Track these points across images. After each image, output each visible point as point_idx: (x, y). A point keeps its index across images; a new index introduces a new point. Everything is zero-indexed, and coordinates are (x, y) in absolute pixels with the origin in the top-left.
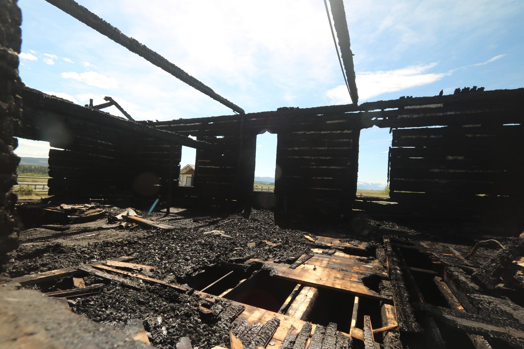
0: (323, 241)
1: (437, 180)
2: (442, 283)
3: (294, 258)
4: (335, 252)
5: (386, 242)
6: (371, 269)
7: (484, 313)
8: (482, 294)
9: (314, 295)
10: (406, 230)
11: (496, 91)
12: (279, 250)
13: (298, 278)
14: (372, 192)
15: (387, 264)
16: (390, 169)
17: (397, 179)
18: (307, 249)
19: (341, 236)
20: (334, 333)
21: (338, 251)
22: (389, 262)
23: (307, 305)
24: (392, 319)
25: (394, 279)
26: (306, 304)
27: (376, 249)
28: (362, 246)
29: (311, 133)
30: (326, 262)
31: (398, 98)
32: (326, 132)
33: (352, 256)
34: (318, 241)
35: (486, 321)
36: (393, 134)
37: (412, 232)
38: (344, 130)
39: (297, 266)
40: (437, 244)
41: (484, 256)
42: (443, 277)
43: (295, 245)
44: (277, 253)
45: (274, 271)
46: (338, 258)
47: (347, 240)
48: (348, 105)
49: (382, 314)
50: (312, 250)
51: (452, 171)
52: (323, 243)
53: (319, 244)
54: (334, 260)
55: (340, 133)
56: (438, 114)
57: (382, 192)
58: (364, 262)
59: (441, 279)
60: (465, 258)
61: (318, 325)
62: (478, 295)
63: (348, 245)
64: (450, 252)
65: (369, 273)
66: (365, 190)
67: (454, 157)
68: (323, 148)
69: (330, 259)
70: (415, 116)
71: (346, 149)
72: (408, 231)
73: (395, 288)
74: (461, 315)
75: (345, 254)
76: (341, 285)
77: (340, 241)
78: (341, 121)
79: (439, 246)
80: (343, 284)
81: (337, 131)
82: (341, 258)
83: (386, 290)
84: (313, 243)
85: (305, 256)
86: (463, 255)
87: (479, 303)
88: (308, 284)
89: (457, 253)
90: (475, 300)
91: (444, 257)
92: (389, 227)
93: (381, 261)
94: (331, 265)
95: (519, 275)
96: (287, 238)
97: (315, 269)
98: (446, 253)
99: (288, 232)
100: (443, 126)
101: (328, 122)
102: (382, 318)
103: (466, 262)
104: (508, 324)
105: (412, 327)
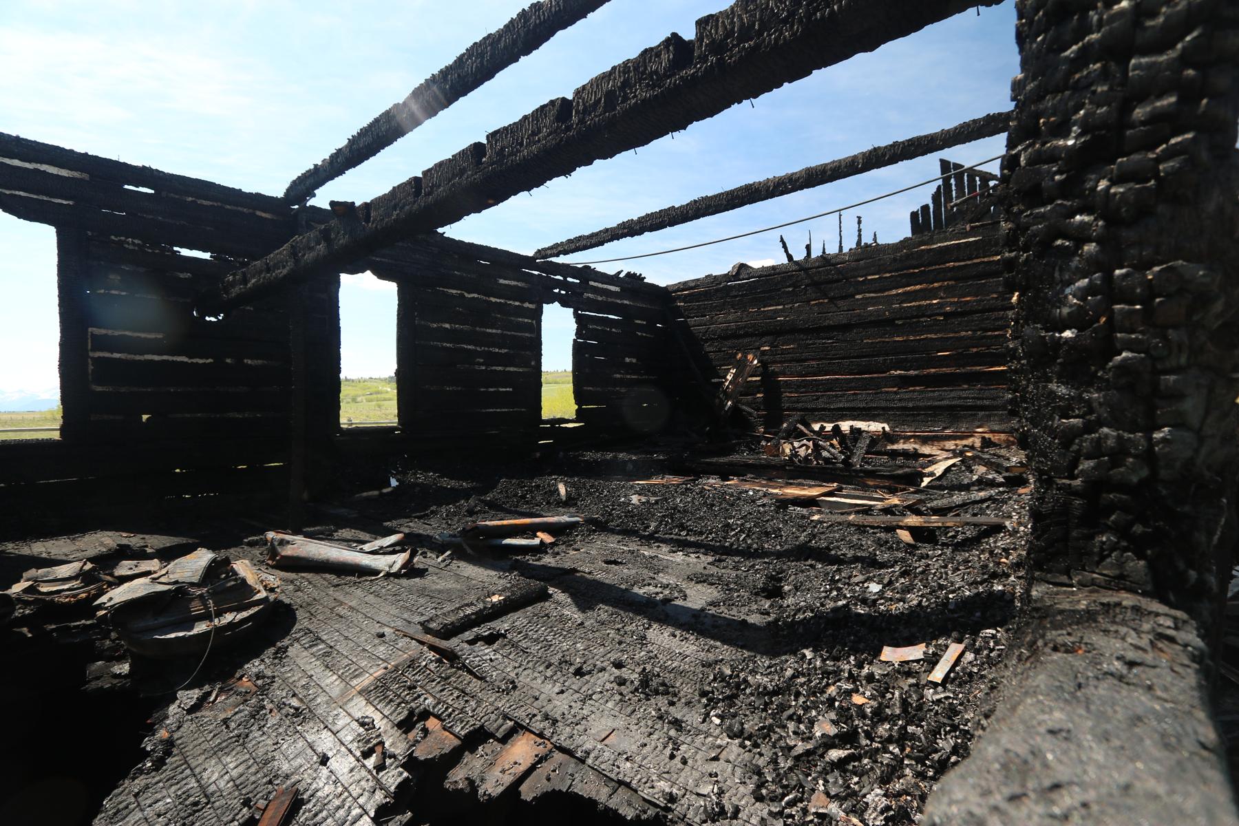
11: (197, 180)
57: (49, 416)
68: (494, 331)
81: (515, 300)
100: (616, 318)
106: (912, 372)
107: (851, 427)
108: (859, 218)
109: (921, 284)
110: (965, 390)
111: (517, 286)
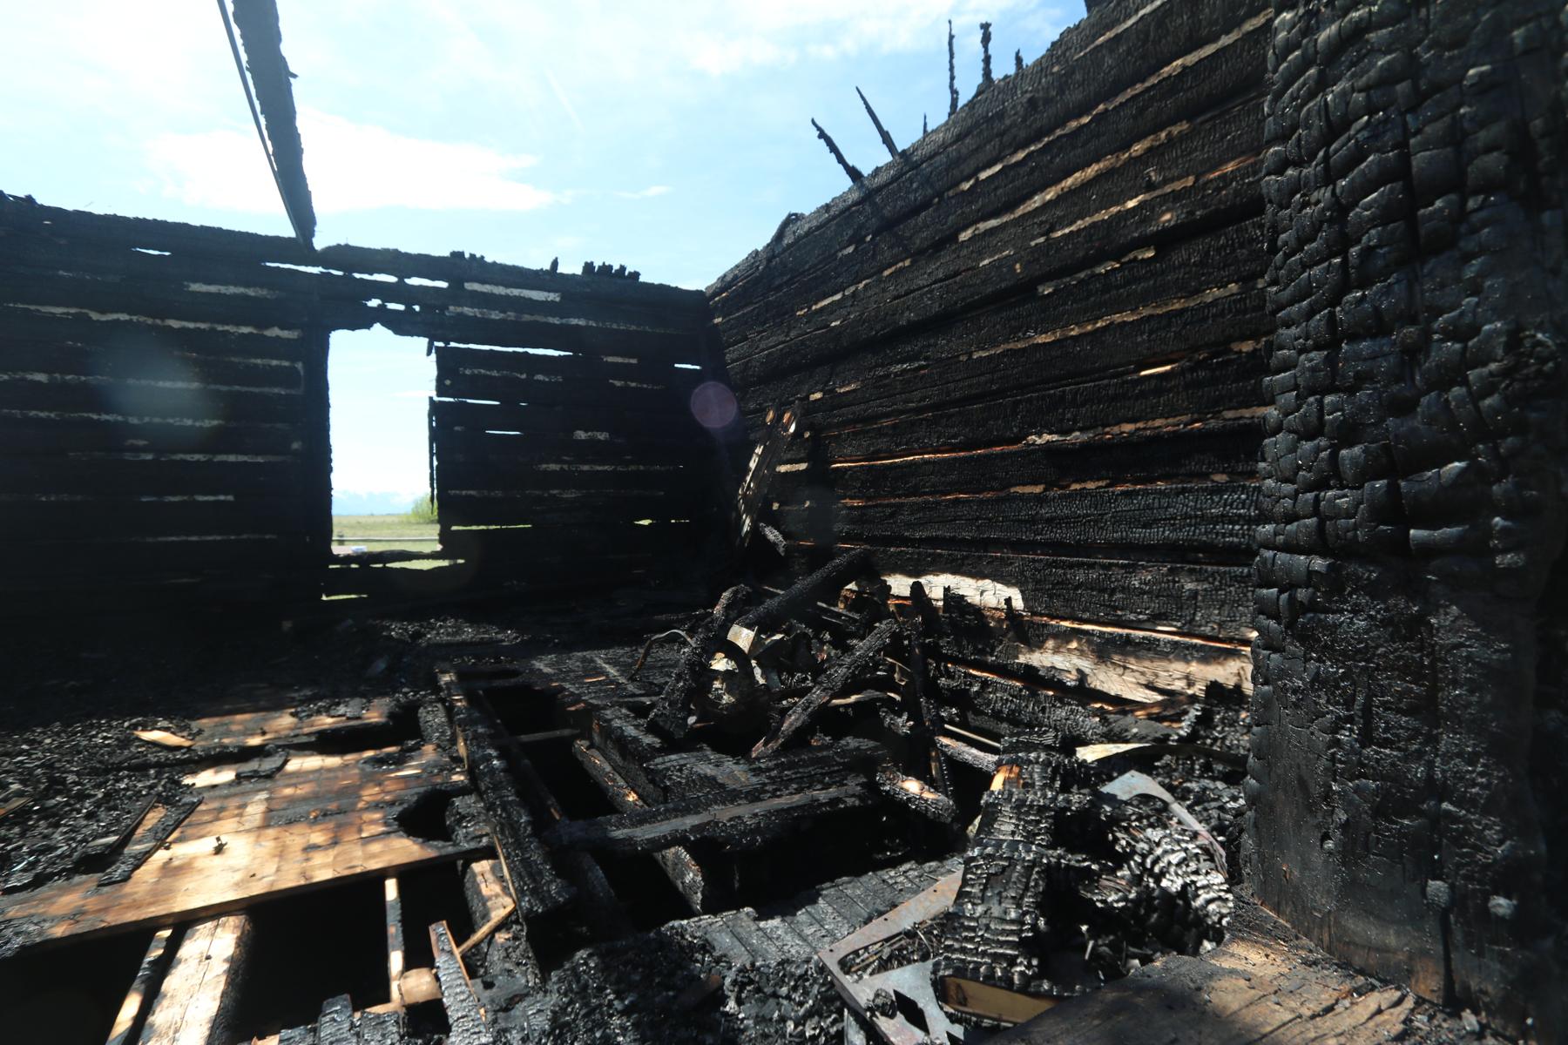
0: (228, 734)
1: (555, 492)
3: (112, 839)
4: (286, 762)
5: (446, 683)
6: (417, 777)
8: (667, 755)
9: (240, 942)
10: (493, 633)
12: (17, 830)
13: (153, 909)
14: (372, 520)
15: (461, 749)
16: (435, 463)
17: (458, 492)
18: (164, 786)
19: (293, 699)
20: (346, 1025)
21: (296, 756)
22: (465, 744)
23: (221, 987)
24: (497, 896)
25: (489, 788)
26: (215, 988)
27: (419, 707)
28: (375, 714)
29: (118, 320)
30: (262, 808)
31: (446, 254)
32: (191, 325)
33: (350, 757)
34: (206, 739)
35: (680, 811)
36: (437, 358)
37: (509, 636)
38: (267, 327)
39: (137, 867)
40: (570, 659)
41: (659, 664)
42: (590, 738)
43: (98, 786)
44: (9, 848)
45: (18, 930)
46: (301, 780)
47: (321, 707)
48: (277, 238)
49: (469, 893)
50: (188, 780)
51: (586, 468)
52: (226, 741)
53: (215, 748)
54: (288, 791)
55: (251, 334)
56: (551, 320)
57: (405, 520)
58: (391, 765)
59: (586, 743)
60: (628, 680)
61: (285, 1033)
63: (326, 722)
64: (599, 672)
65: (411, 795)
66: (347, 516)
67: (589, 433)
69: (271, 791)
70: (495, 315)
71: (283, 393)
72: (500, 636)
73: (495, 811)
74: (641, 819)
75: (324, 757)
76: (333, 865)
77: (293, 715)
78: (251, 292)
79: (574, 661)
80: (339, 859)
81: (238, 324)
82: (311, 777)
83: (469, 822)
84: (184, 754)
85: (166, 815)
86: (624, 671)
88: (203, 914)
89: (612, 671)
92: (448, 634)
93: (442, 744)
94: (281, 813)
95: (717, 689)
96: (48, 766)
97: (219, 850)
99: (48, 741)
100: (562, 353)
101: (196, 287)
102: (470, 905)
103: (631, 687)
105: (550, 895)
106: (1076, 437)
107: (947, 590)
108: (985, 27)
109: (1098, 161)
110: (1218, 490)
111: (246, 297)
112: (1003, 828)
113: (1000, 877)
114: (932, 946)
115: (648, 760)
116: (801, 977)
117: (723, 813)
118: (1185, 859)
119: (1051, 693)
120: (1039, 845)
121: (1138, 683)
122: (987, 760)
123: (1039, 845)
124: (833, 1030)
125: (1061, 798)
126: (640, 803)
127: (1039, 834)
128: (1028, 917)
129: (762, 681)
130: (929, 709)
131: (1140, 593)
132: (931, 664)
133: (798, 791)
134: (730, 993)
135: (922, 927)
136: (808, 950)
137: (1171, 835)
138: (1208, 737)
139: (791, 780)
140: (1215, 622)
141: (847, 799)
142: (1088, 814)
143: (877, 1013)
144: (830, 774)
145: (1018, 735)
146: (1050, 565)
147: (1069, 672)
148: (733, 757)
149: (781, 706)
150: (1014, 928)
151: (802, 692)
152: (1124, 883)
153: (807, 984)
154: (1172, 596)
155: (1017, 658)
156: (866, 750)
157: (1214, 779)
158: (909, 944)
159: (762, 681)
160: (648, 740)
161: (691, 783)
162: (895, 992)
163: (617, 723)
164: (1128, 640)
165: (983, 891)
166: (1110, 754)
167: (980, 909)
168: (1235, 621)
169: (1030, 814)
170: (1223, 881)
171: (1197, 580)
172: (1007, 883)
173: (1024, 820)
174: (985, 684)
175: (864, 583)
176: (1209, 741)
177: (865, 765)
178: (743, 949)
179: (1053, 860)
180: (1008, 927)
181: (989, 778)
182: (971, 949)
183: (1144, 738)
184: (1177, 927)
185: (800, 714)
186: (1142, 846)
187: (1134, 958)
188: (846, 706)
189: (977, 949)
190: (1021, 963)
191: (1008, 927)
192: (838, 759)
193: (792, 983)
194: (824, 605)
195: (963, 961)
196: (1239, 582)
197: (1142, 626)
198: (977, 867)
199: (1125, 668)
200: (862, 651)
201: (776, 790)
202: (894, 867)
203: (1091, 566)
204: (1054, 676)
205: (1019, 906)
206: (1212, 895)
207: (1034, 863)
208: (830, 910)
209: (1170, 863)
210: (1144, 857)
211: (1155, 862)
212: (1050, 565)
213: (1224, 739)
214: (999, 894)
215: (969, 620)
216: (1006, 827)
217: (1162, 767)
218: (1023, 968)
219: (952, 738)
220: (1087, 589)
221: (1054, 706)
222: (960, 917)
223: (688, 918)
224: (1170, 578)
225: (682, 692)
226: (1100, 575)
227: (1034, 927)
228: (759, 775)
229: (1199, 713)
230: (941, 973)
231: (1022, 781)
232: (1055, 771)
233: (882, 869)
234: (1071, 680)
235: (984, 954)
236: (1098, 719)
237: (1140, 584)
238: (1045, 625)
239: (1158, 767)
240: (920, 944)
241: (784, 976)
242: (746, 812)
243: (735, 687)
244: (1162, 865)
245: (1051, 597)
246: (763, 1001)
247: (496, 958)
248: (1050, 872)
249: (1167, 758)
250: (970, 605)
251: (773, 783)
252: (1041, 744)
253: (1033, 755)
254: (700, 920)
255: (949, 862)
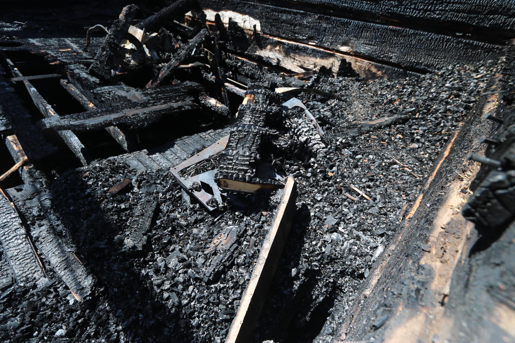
2: (69, 85)
7: (106, 105)
35: (109, 112)
42: (67, 79)
59: (66, 81)
60: (83, 51)
62: (99, 89)
64: (67, 46)
79: (53, 41)
87: (102, 96)
89: (75, 46)
90: (98, 94)
91: (62, 54)
95: (128, 58)
98: (63, 48)
103: (85, 55)
104: (124, 107)
107: (230, 19)
112: (246, 119)
113: (243, 139)
114: (216, 164)
115: (93, 89)
116: (165, 176)
117: (129, 113)
118: (309, 130)
119: (266, 68)
120: (259, 126)
121: (298, 65)
122: (241, 92)
123: (259, 126)
124: (177, 195)
125: (269, 107)
126: (95, 108)
127: (259, 122)
128: (253, 154)
129: (149, 55)
130: (221, 72)
131: (306, 27)
132: (223, 53)
133: (164, 103)
134: (135, 185)
135: (212, 157)
136: (170, 164)
137: (305, 121)
138: (317, 86)
139: (162, 99)
140: (329, 42)
141: (186, 107)
142: (278, 114)
143: (194, 190)
144: (179, 96)
145: (255, 82)
146: (273, 10)
147: (274, 59)
148: (135, 88)
149: (158, 67)
150: (247, 159)
151: (168, 60)
152: (287, 138)
153: (168, 179)
154: (317, 29)
155: (256, 52)
156: (194, 87)
157: (317, 101)
158: (207, 164)
159: (149, 55)
160: (93, 79)
161: (114, 99)
162: (201, 182)
163: (76, 71)
164: (297, 47)
165: (237, 145)
166: (285, 91)
167: (235, 152)
168: (336, 42)
169: (257, 114)
170: (320, 137)
171: (328, 23)
172: (246, 141)
173: (254, 116)
174: (243, 63)
175: (195, 13)
176: (317, 88)
177: (194, 93)
178: (143, 166)
179: (264, 132)
180: (245, 159)
181: (242, 99)
182: (231, 168)
183: (296, 86)
184: (303, 154)
185: (166, 71)
186: (294, 125)
187: (287, 164)
188: (188, 68)
189: (233, 168)
190: (249, 172)
191: (245, 159)
192: (182, 90)
193: (162, 178)
194: (178, 22)
195: (227, 173)
196: (342, 25)
197: (303, 42)
198: (235, 135)
199: (294, 59)
200: (193, 43)
201: (155, 102)
202: (205, 131)
203: (289, 13)
204: (268, 61)
205: (250, 150)
206: (316, 142)
207: (257, 133)
208: (179, 149)
209: (303, 131)
210: (295, 129)
211: (298, 131)
212: (273, 10)
213: (322, 87)
214: (243, 146)
215: (238, 34)
216: (247, 119)
217: (300, 96)
218: (249, 174)
219: (229, 83)
220: (286, 23)
221: (267, 73)
222: (227, 155)
223: (117, 155)
224: (318, 21)
225: (106, 57)
226: (292, 17)
227: (255, 158)
228: (147, 96)
229: (316, 78)
230: (218, 178)
231: (254, 101)
232: (267, 97)
233: (200, 132)
234: (274, 62)
235: (235, 169)
236: (282, 78)
237: (306, 23)
238: (268, 39)
239: (299, 96)
240: (211, 164)
241: (159, 176)
242: (141, 112)
243: (136, 57)
244: (300, 131)
245: (271, 26)
246: (150, 186)
247: (26, 177)
248: (263, 137)
249: (303, 93)
250: (239, 27)
251: (154, 99)
252: (263, 86)
253: (259, 91)
254: (123, 156)
255: (226, 129)
